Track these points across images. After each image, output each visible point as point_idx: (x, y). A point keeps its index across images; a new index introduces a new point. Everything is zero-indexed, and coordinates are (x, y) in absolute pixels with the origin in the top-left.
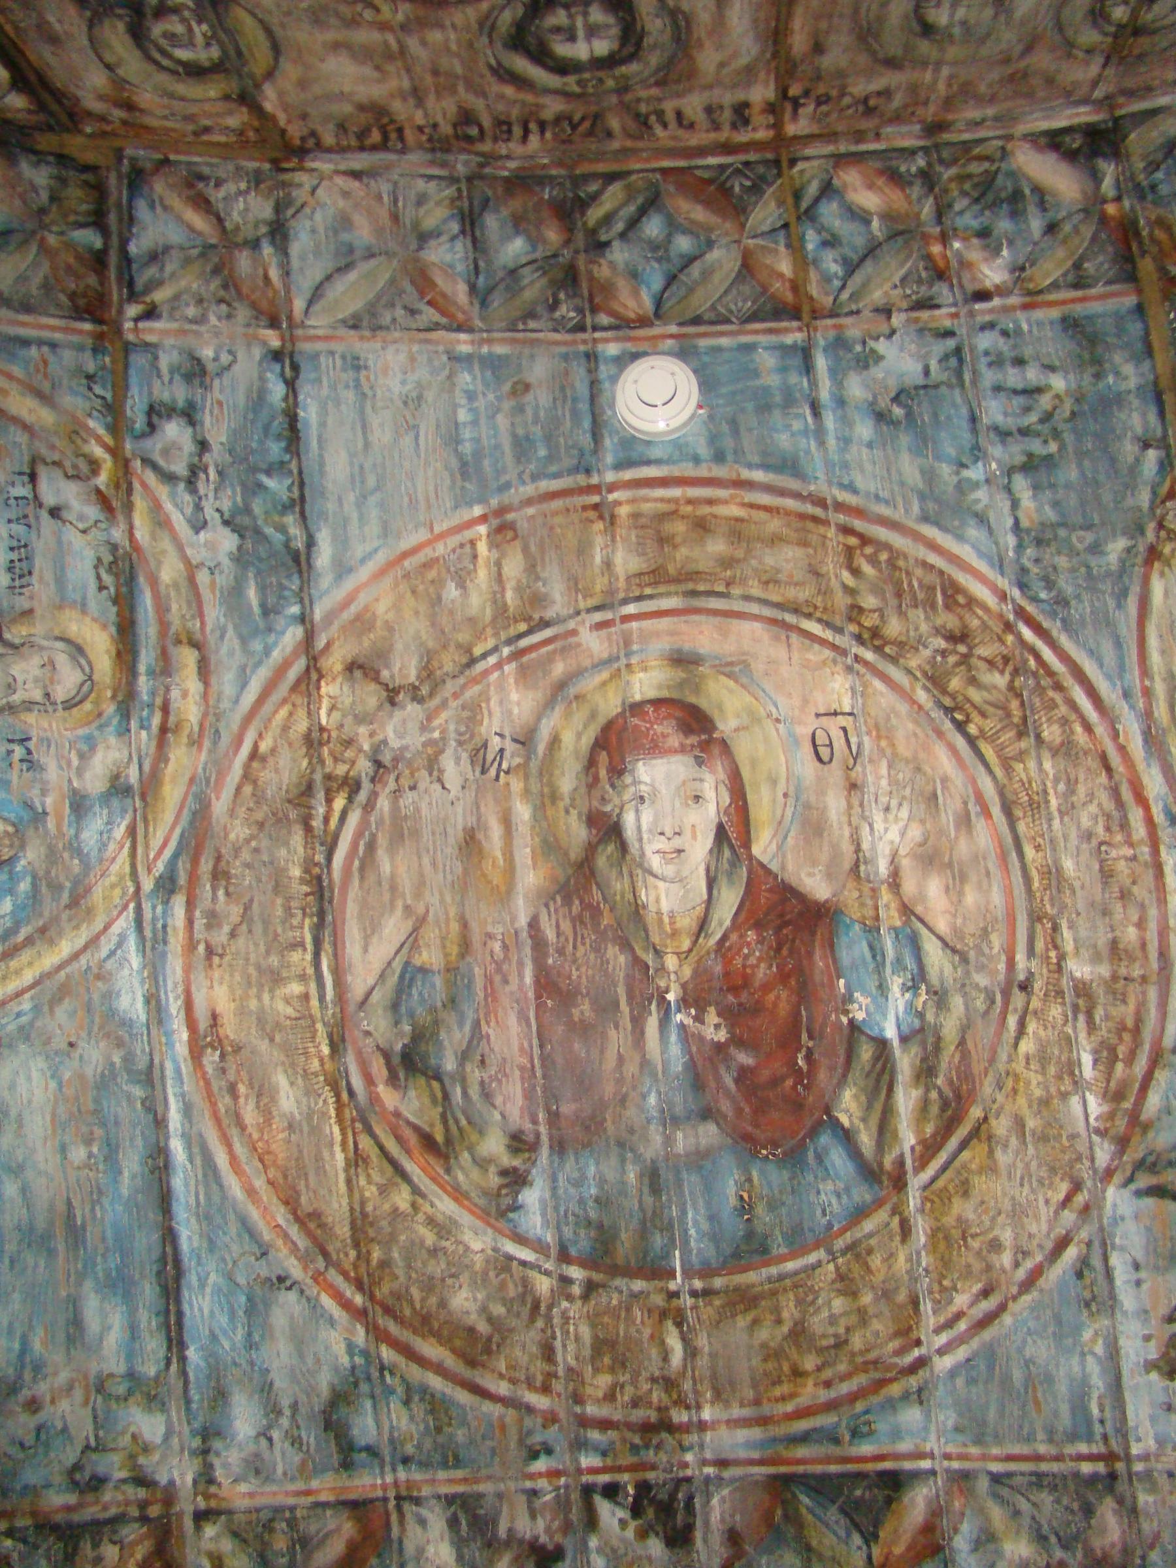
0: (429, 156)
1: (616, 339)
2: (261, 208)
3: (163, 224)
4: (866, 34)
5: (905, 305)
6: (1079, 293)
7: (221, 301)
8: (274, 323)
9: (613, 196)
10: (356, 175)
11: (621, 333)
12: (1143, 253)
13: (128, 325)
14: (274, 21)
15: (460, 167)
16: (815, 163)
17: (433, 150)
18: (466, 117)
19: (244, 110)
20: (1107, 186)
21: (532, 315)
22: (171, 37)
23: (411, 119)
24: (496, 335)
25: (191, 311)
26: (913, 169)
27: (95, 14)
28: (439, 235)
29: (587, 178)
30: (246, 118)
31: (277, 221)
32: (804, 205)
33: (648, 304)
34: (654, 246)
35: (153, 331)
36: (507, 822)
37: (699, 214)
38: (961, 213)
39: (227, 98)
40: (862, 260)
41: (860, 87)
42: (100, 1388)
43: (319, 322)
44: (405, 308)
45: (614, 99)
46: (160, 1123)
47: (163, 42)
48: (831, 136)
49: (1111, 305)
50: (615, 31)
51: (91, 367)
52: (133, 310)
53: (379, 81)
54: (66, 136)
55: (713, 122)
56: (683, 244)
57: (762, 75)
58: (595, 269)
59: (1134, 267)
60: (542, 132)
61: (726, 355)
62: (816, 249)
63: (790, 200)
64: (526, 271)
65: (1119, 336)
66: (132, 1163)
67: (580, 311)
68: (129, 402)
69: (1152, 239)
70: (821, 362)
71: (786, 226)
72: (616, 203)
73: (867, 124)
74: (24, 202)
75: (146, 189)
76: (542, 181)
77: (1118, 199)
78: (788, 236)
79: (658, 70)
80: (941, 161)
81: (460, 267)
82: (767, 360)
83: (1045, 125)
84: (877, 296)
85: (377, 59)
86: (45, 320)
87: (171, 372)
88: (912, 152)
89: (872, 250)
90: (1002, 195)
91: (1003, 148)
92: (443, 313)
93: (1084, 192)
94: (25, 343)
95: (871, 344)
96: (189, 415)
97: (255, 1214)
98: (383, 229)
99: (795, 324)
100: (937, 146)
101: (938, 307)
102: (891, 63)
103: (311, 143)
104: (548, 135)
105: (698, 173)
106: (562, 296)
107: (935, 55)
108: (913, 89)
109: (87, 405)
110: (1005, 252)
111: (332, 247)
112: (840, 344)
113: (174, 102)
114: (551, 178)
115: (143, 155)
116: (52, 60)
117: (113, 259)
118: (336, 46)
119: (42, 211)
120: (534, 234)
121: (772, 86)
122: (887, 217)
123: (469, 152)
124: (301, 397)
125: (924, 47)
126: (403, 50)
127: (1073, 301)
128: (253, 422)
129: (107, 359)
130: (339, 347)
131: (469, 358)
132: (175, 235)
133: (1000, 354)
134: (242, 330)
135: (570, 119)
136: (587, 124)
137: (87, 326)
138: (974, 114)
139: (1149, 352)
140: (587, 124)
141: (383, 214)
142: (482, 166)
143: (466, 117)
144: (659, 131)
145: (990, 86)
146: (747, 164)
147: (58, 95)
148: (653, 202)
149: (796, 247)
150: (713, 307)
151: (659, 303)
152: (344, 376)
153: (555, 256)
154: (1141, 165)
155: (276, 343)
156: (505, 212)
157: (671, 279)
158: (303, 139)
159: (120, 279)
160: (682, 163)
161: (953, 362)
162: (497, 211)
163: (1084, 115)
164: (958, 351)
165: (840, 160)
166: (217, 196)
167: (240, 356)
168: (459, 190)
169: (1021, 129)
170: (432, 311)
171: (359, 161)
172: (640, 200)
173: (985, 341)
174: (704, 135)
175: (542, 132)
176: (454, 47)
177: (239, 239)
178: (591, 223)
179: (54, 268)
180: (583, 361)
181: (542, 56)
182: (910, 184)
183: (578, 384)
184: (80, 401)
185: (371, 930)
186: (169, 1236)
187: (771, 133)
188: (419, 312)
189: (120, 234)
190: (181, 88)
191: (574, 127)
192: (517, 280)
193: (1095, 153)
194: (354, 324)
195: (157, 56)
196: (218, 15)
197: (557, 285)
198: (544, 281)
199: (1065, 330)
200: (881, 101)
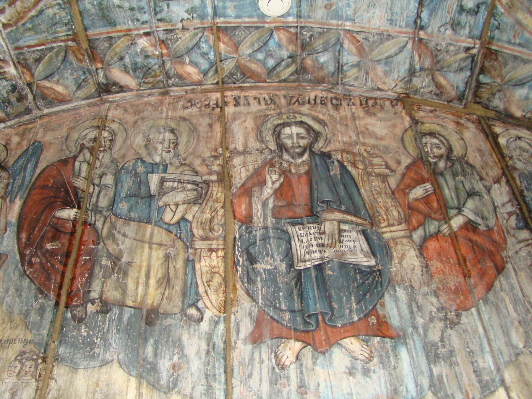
0: (351, 93)
1: (288, 22)
2: (417, 82)
3: (455, 80)
4: (194, 130)
5: (177, 31)
6: (109, 35)
7: (439, 51)
8: (421, 40)
9: (286, 73)
10: (379, 89)
11: (287, 25)
12: (86, 50)
13: (477, 46)
14: (402, 150)
15: (341, 89)
16: (209, 83)
17: (349, 96)
18: (337, 107)
19: (416, 118)
20: (101, 74)
21: (320, 34)
22: (439, 148)
23: (357, 109)
24: (335, 28)
25: (452, 48)
26: (173, 79)
27: (463, 158)
28: (352, 66)
29: (294, 81)
30: (417, 115)
31: (412, 77)
32: (214, 68)
33: (275, 35)
34: (271, 55)
35: (469, 43)
37: (253, 66)
38: (155, 64)
39: (422, 123)
40: (193, 48)
41: (194, 110)
43: (403, 39)
44: (369, 41)
45: (283, 110)
47: (442, 146)
48: (204, 92)
49: (97, 31)
50: (283, 136)
51: (496, 32)
52: (474, 51)
53: (368, 124)
54: (484, 115)
55: (247, 100)
56: (260, 56)
57: (230, 117)
58: (294, 49)
59: (89, 46)
60: (309, 99)
61: (247, 15)
62: (210, 52)
63: (219, 70)
64: (321, 50)
65: (94, 19)
67: (301, 34)
68: (485, 17)
69: (83, 55)
70: (210, 10)
71: (221, 61)
72: (284, 72)
73: (191, 96)
74: (505, 95)
75: (459, 93)
76: (311, 81)
77: (97, 69)
78: (220, 57)
79: (267, 121)
80: (163, 82)
81: (345, 53)
82: (231, 12)
83: (125, 94)
84: (187, 35)
85: (366, 132)
86: (510, 52)
87: (465, 27)
88: (173, 85)
89: (189, 51)
90: (140, 70)
91: (140, 86)
92: (354, 37)
93: (110, 72)
94: (520, 45)
95: (190, 17)
98: (372, 70)
99: (219, 25)
100: (165, 88)
101: (164, 30)
102: (184, 119)
103: (394, 103)
104: (307, 98)
105: (252, 81)
106: (308, 40)
107: (168, 122)
108: (175, 109)
109: (502, 18)
110: (139, 50)
111: (393, 65)
112: (202, 17)
113: (441, 123)
114: (307, 82)
115: (456, 105)
116: (482, 143)
117: (477, 70)
118: (381, 139)
119: (499, 91)
120: (316, 63)
121: (226, 112)
122: (183, 63)
123: (336, 93)
124: (416, 11)
125: (173, 125)
126: (358, 135)
127: (112, 32)
128: (437, 4)
129: (489, 34)
130: (397, 29)
131: (347, 20)
132: (451, 76)
133: (140, 12)
134: (433, 39)
135: (299, 104)
136: (293, 101)
137: (494, 47)
138: (152, 99)
139: (81, 13)
140: (293, 101)
141: (371, 75)
142: (332, 88)
143: (337, 107)
144: (267, 97)
145: (147, 109)
146: (234, 83)
147: (483, 131)
148: (271, 71)
149: (218, 53)
150: (250, 33)
151: (271, 35)
152: (397, 18)
153: (309, 55)
154: (89, 81)
155: (421, 33)
156: (326, 71)
157: (266, 44)
158: (397, 104)
159: (476, 63)
160: (258, 84)
161: (158, 9)
162: (329, 72)
163: (111, 97)
164: (156, 14)
165: (200, 83)
166: (432, 88)
167: (436, 30)
168: (342, 80)
169: (134, 93)
170: (359, 39)
171: (377, 94)
172: (275, 72)
173: (146, 17)
174: (250, 94)
175: (309, 99)
176: (340, 135)
177: (427, 72)
178: (294, 65)
179: (501, 70)
180: (302, 15)
181: (309, 129)
182: (174, 75)
183: (306, 6)
184: (505, 19)
187: (225, 94)
188: (363, 38)
189: (472, 79)
190: (438, 128)
191: (298, 100)
192: (324, 47)
193: (107, 85)
194: (389, 37)
195: (444, 141)
196: (421, 153)
197: (309, 44)
198: (314, 46)
199: (114, 21)
200: (186, 105)
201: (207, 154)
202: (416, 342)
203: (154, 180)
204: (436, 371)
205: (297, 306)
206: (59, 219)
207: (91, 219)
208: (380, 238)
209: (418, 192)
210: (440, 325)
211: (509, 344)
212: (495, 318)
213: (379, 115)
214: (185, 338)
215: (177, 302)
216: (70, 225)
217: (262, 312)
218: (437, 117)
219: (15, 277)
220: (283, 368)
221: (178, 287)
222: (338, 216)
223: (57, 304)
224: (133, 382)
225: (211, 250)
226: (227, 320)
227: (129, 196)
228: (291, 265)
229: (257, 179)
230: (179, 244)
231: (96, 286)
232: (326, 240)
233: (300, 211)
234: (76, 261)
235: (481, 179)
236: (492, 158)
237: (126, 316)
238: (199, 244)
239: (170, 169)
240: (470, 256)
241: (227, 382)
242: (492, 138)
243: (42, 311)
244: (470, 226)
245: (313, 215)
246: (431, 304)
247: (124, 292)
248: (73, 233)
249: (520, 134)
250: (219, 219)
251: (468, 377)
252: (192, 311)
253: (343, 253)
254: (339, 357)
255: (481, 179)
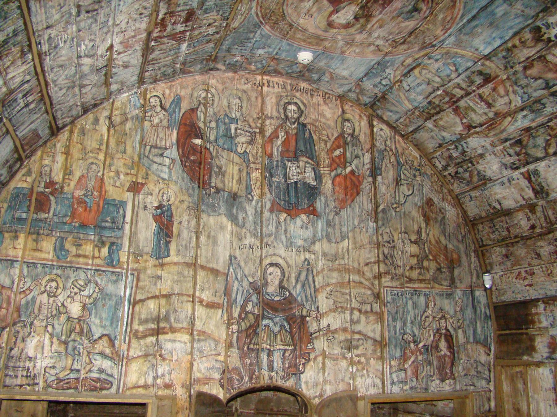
35: (378, 92)
36: (373, 26)
41: (249, 86)
42: (511, 5)
46: (464, 25)
66: (474, 24)
96: (380, 83)
97: (462, 7)
108: (240, 84)
118: (328, 120)
143: (312, 95)
147: (369, 122)
171: (330, 92)
185: (407, 27)
186: (478, 13)
190: (352, 118)
201: (255, 116)
202: (324, 219)
203: (233, 127)
204: (328, 230)
205: (287, 199)
206: (194, 144)
207: (208, 146)
208: (320, 173)
209: (337, 153)
210: (333, 213)
211: (353, 223)
212: (351, 214)
213: (330, 105)
214: (247, 207)
215: (244, 191)
216: (199, 148)
217: (274, 199)
218: (353, 110)
219: (180, 172)
220: (280, 223)
221: (244, 185)
222: (305, 159)
223: (199, 187)
224: (230, 223)
225: (256, 169)
226: (262, 201)
227: (223, 136)
228: (286, 181)
229: (275, 136)
230: (244, 164)
231: (213, 180)
232: (299, 171)
233: (291, 154)
234: (204, 167)
235: (362, 149)
236: (368, 139)
237: (226, 196)
238: (252, 165)
239: (240, 122)
240: (349, 186)
241: (261, 226)
242: (371, 126)
243: (193, 189)
244: (352, 172)
245: (296, 158)
246: (332, 205)
247: (224, 185)
248: (201, 153)
249: (383, 128)
250: (260, 154)
251: (338, 234)
252: (249, 196)
253: (305, 178)
254: (299, 221)
255: (362, 149)
